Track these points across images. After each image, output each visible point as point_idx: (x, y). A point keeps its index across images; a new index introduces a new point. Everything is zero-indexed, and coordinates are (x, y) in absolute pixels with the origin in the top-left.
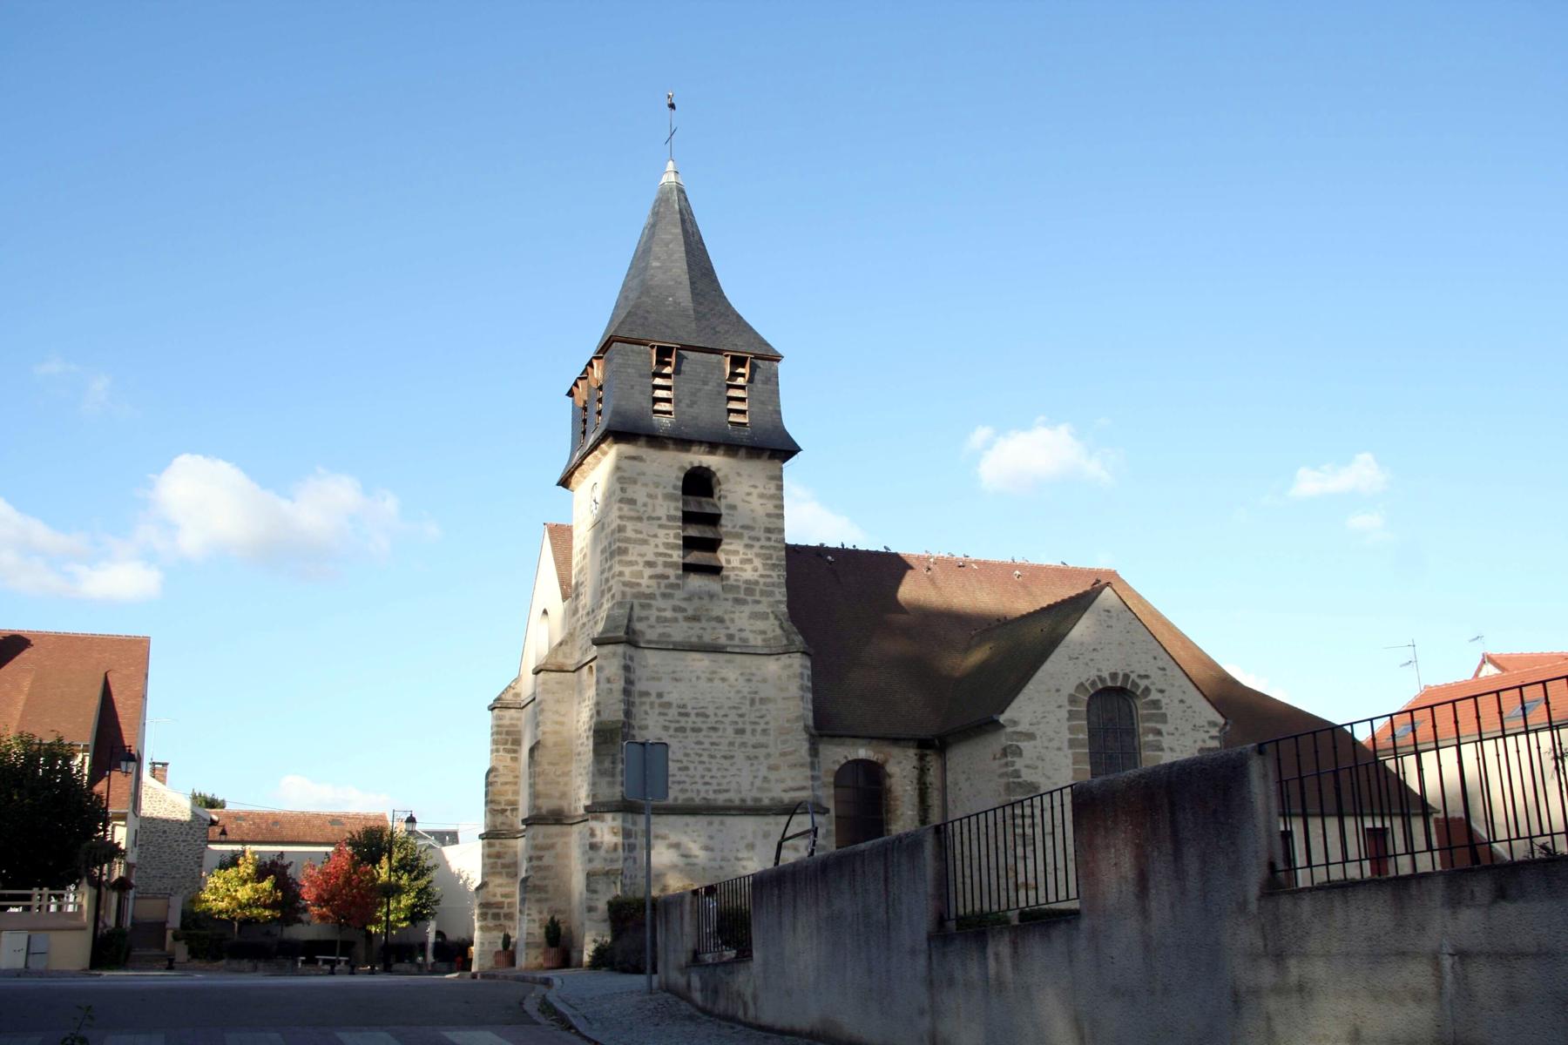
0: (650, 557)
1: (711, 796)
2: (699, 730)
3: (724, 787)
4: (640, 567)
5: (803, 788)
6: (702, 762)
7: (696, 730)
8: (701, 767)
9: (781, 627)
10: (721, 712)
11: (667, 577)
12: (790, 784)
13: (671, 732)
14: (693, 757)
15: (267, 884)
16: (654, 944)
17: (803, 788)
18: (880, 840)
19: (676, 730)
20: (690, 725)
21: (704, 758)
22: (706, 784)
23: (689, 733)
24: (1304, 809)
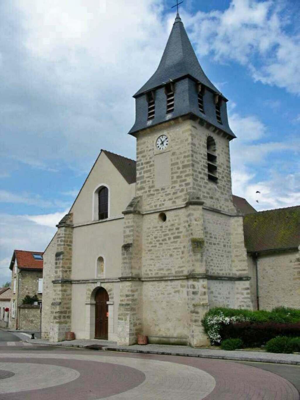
0: (200, 170)
5: (244, 270)
18: (212, 135)
22: (218, 267)
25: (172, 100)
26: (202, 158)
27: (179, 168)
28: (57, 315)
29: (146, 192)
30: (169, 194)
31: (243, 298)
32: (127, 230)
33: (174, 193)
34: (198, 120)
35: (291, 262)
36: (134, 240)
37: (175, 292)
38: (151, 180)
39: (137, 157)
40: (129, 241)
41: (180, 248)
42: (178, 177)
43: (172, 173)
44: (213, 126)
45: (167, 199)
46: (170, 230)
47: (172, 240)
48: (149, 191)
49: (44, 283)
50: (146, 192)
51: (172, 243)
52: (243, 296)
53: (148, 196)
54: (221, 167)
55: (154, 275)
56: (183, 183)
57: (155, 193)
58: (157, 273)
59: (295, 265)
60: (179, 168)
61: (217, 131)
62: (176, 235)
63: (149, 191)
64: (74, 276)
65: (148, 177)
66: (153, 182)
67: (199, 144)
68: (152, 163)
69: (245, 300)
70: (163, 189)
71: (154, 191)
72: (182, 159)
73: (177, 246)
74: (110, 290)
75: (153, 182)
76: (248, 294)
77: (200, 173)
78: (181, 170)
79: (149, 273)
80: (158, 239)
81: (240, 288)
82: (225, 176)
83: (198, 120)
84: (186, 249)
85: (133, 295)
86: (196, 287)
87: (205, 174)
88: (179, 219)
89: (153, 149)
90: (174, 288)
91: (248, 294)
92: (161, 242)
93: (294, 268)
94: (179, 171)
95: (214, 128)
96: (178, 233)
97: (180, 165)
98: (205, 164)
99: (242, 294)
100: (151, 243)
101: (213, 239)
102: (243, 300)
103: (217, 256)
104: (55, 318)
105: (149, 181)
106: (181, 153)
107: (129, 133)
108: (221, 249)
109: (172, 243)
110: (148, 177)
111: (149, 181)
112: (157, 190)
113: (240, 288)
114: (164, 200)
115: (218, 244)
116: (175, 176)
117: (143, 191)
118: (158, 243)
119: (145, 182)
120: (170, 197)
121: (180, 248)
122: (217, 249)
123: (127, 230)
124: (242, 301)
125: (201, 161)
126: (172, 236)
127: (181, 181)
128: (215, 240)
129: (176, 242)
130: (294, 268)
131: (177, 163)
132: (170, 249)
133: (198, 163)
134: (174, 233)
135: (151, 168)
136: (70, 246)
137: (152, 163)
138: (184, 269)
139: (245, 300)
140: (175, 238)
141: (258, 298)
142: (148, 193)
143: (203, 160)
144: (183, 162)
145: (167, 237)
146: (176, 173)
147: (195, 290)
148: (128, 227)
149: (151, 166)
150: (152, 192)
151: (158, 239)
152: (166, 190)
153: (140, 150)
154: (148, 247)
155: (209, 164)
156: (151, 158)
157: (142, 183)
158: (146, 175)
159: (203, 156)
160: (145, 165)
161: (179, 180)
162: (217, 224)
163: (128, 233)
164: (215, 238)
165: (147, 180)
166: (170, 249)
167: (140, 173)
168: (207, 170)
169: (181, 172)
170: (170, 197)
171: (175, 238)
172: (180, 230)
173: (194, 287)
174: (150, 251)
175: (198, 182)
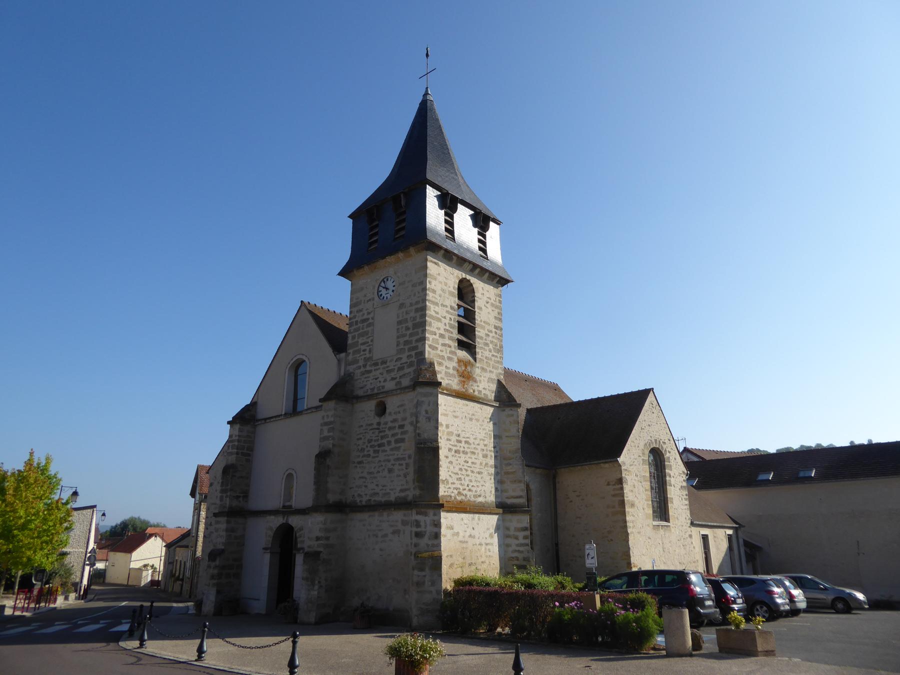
0: (442, 332)
1: (472, 499)
2: (467, 453)
3: (478, 493)
4: (437, 337)
5: (520, 497)
6: (468, 475)
7: (465, 453)
8: (467, 479)
9: (537, 468)
10: (477, 442)
11: (450, 347)
12: (511, 493)
13: (453, 453)
14: (464, 472)
15: (25, 559)
16: (386, 637)
17: (520, 497)
18: (468, 277)
19: (456, 452)
20: (462, 449)
21: (469, 473)
22: (470, 490)
23: (461, 455)
24: (402, 504)
25: (404, 220)
26: (447, 312)
27: (407, 329)
28: (216, 571)
29: (360, 368)
30: (392, 370)
31: (517, 545)
32: (325, 428)
33: (400, 369)
34: (442, 252)
35: (608, 484)
36: (334, 445)
37: (394, 533)
38: (368, 348)
39: (351, 312)
40: (329, 444)
41: (404, 459)
42: (406, 343)
43: (398, 337)
44: (470, 262)
45: (389, 378)
46: (390, 429)
47: (393, 445)
48: (365, 366)
49: (573, 536)
50: (360, 368)
51: (392, 450)
52: (517, 542)
53: (363, 374)
54: (483, 328)
55: (364, 503)
56: (413, 353)
57: (373, 368)
58: (370, 500)
59: (614, 490)
60: (407, 329)
61: (478, 270)
62: (399, 436)
63: (365, 366)
64: (255, 504)
65: (363, 344)
66: (370, 351)
67: (443, 290)
68: (371, 321)
69: (521, 549)
70: (384, 362)
71: (370, 366)
72: (412, 314)
73: (400, 456)
74: (301, 529)
75: (370, 351)
76: (525, 537)
77: (442, 336)
78: (411, 331)
79: (358, 500)
80: (373, 443)
81: (512, 528)
82: (492, 342)
83: (442, 252)
84: (412, 461)
85: (327, 538)
86: (422, 524)
87: (450, 338)
88: (405, 410)
89: (373, 299)
90: (392, 526)
91: (525, 537)
92: (377, 448)
93: (614, 496)
94: (408, 332)
95: (471, 266)
96: (402, 433)
97: (410, 324)
98: (452, 322)
99: (517, 538)
100: (363, 450)
101: (463, 444)
102: (517, 549)
103: (469, 473)
104: (212, 577)
105: (490, 371)
106: (411, 305)
107: (339, 274)
108: (478, 462)
109: (392, 450)
110: (363, 344)
111: (364, 350)
112: (376, 364)
113: (512, 528)
114: (385, 381)
115: (473, 453)
116: (402, 340)
117: (355, 366)
118: (372, 450)
119: (359, 351)
120: (393, 375)
121: (404, 459)
122: (470, 461)
123: (325, 428)
124: (516, 551)
125: (445, 318)
126: (393, 440)
127: (409, 350)
128: (466, 446)
129: (398, 449)
130: (614, 496)
131: (406, 321)
132: (389, 461)
133: (439, 320)
134: (393, 435)
135: (369, 329)
136: (249, 455)
137: (371, 321)
138: (408, 493)
139: (521, 549)
140: (397, 441)
141: (557, 545)
142: (362, 369)
143: (448, 316)
144: (414, 319)
145: (385, 441)
146: (404, 336)
147: (419, 530)
148: (326, 424)
149: (369, 326)
150: (368, 368)
151: (373, 443)
152: (388, 364)
153: (355, 301)
154: (359, 456)
155: (459, 322)
156: (369, 313)
157: (355, 352)
158: (361, 341)
159: (449, 309)
160: (360, 325)
161: (406, 347)
162: (471, 419)
163: (326, 434)
164: (466, 442)
165: (363, 347)
166: (389, 461)
167: (353, 338)
168: (455, 331)
169: (411, 335)
170: (393, 375)
171: (397, 441)
172: (406, 428)
173: (418, 524)
174: (360, 463)
175: (438, 352)
